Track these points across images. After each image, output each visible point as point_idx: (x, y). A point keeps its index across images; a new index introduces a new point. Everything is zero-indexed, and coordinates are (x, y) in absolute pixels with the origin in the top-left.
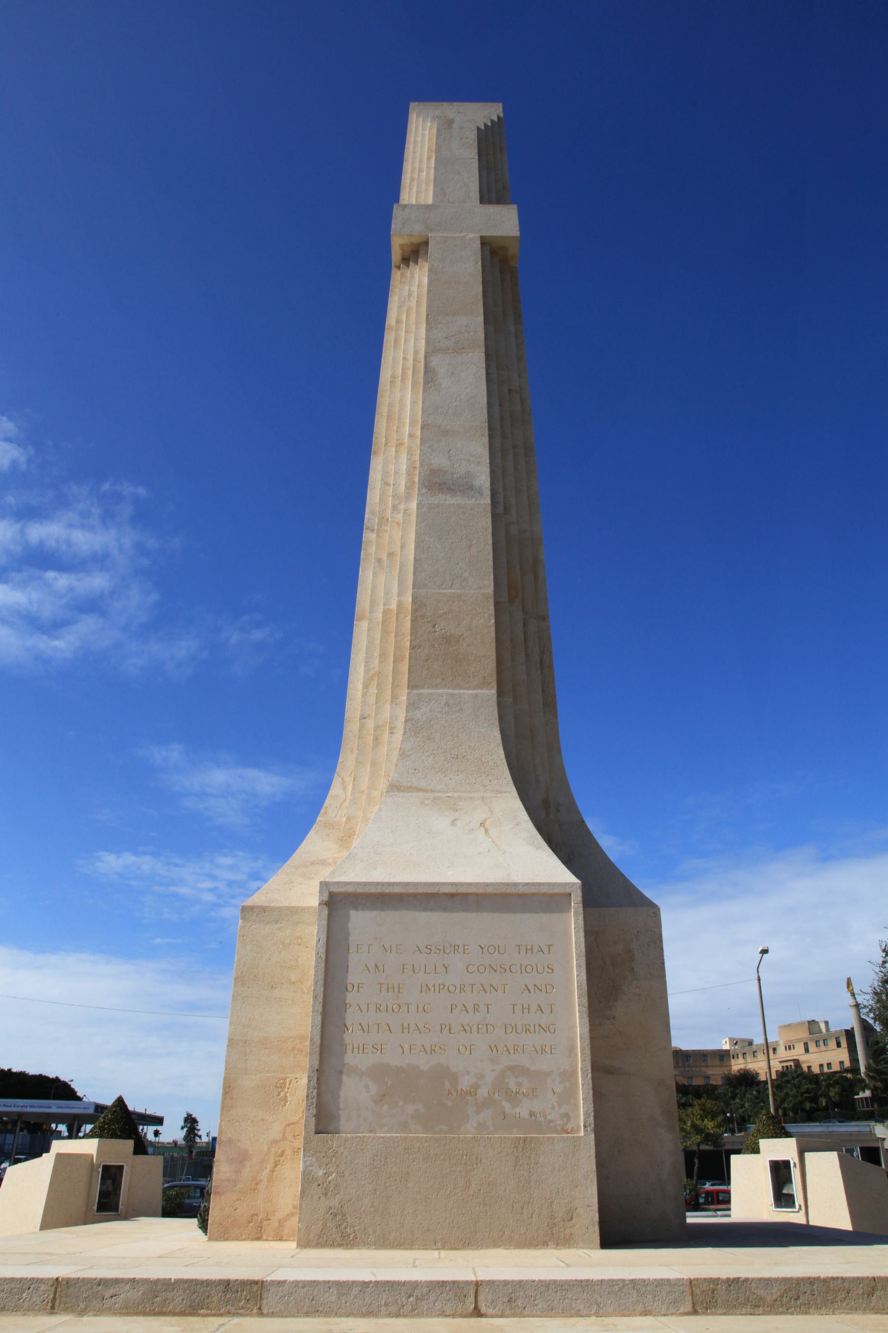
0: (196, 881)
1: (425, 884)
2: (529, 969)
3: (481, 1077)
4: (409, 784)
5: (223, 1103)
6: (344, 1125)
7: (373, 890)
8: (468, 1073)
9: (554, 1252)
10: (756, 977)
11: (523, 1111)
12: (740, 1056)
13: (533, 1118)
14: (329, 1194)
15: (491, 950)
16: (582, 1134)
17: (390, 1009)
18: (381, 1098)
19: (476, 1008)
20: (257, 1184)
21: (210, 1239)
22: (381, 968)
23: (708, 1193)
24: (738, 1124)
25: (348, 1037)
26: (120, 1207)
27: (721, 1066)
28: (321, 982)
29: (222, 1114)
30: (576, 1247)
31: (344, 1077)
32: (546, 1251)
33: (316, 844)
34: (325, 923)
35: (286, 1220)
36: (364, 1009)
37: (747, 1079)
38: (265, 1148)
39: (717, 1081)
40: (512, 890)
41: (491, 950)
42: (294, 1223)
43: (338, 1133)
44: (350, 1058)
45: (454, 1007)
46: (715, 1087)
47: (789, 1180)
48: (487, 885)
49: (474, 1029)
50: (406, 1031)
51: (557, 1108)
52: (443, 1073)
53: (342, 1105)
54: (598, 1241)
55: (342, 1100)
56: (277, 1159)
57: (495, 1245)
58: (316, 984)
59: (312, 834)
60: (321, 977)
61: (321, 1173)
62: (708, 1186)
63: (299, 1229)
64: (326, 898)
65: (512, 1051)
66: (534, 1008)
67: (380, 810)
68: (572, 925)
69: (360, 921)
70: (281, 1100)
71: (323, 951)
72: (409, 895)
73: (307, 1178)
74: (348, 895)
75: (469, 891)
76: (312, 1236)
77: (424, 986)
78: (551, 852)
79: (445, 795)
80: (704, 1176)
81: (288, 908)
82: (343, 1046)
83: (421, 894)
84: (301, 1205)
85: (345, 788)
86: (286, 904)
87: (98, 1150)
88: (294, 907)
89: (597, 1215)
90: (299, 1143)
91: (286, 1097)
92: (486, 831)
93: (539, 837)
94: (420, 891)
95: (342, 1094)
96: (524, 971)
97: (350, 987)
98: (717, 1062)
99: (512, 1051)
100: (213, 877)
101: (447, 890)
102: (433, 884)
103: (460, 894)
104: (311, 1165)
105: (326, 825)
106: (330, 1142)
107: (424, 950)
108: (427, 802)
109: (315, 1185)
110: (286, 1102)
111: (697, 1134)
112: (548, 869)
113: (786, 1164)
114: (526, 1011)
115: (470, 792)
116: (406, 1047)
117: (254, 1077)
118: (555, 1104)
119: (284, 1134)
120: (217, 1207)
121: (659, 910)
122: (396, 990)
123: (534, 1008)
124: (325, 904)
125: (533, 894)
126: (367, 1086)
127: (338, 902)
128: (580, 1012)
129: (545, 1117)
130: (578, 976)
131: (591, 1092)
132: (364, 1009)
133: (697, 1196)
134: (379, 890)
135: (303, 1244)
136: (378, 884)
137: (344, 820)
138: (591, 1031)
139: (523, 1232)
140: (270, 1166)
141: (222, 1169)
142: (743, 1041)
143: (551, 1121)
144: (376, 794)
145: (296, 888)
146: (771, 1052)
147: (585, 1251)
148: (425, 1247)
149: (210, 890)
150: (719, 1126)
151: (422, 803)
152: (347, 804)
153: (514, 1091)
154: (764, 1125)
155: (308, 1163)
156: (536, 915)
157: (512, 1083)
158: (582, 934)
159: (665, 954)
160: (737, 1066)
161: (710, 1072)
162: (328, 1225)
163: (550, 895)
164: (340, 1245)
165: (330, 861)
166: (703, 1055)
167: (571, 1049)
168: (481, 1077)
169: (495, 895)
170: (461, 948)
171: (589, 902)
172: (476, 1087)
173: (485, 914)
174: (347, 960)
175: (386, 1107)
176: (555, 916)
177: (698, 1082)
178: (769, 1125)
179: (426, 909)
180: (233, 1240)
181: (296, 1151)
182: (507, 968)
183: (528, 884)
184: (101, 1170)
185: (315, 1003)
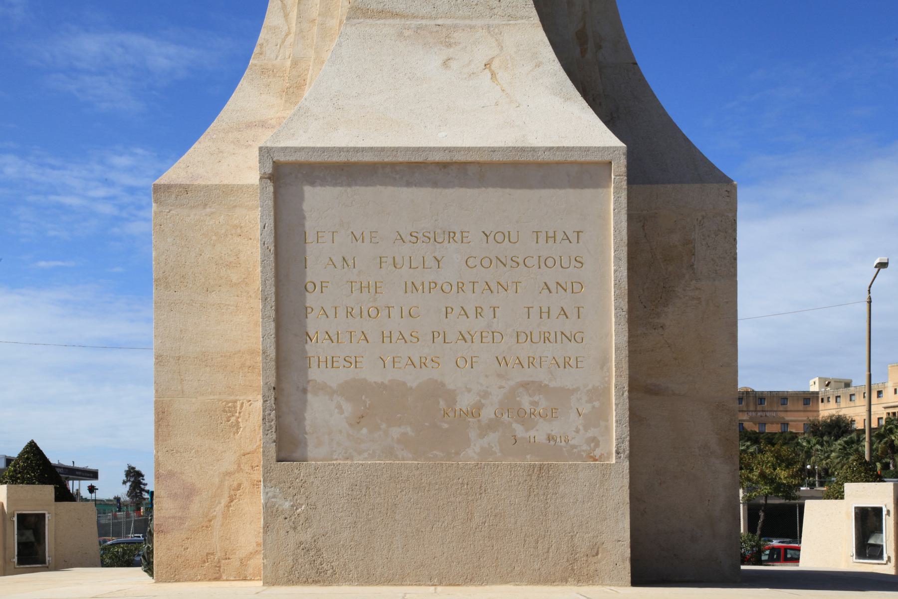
0: (83, 187)
1: (407, 149)
2: (550, 262)
3: (486, 395)
4: (380, 7)
5: (157, 431)
6: (311, 451)
7: (335, 159)
8: (469, 390)
9: (575, 589)
10: (866, 299)
11: (539, 433)
12: (832, 400)
13: (552, 443)
14: (299, 528)
15: (499, 237)
16: (614, 461)
17: (365, 313)
18: (359, 420)
19: (479, 312)
20: (210, 521)
21: (158, 581)
22: (351, 263)
23: (773, 550)
24: (820, 477)
25: (310, 348)
26: (47, 559)
27: (805, 411)
28: (271, 281)
29: (157, 444)
30: (602, 584)
31: (310, 396)
32: (565, 587)
33: (249, 100)
34: (271, 203)
35: (249, 559)
36: (331, 313)
37: (839, 427)
38: (216, 480)
39: (796, 428)
40: (530, 158)
41: (499, 237)
42: (258, 561)
43: (305, 460)
44: (315, 374)
45: (449, 310)
46: (794, 436)
47: (879, 529)
48: (493, 150)
49: (477, 338)
50: (387, 340)
51: (582, 431)
52: (435, 392)
53: (308, 428)
54: (628, 578)
55: (308, 423)
56: (232, 493)
57: (503, 579)
58: (264, 283)
59: (244, 84)
60: (271, 274)
61: (287, 505)
62: (775, 543)
63: (265, 566)
64: (269, 170)
65: (526, 365)
66: (555, 312)
67: (340, 45)
68: (611, 204)
69: (317, 201)
70: (231, 426)
71: (270, 240)
72: (384, 165)
73: (270, 512)
74: (299, 166)
75: (469, 159)
76: (281, 572)
77: (409, 285)
78: (585, 104)
79: (433, 22)
80: (769, 533)
81: (217, 187)
82: (305, 357)
83: (401, 163)
84: (264, 540)
85: (286, 16)
86: (216, 181)
87: (8, 498)
88: (228, 186)
89: (629, 551)
90: (258, 475)
91: (238, 422)
92: (493, 75)
93: (569, 83)
94: (400, 159)
95: (308, 416)
96: (542, 265)
97: (310, 287)
98: (801, 406)
99: (526, 365)
100: (107, 183)
101: (437, 157)
102: (418, 149)
103: (455, 163)
104: (274, 497)
105: (264, 71)
106: (296, 471)
107: (408, 238)
108: (407, 33)
109: (281, 518)
110: (238, 428)
111: (766, 484)
112: (581, 128)
113: (878, 511)
114: (545, 315)
115: (469, 18)
116: (389, 360)
117: (194, 400)
118: (581, 427)
119: (239, 466)
120: (161, 549)
121: (735, 188)
122: (372, 290)
123: (555, 312)
124: (269, 178)
125: (558, 163)
126: (339, 407)
127: (287, 176)
128: (616, 317)
129: (567, 441)
130: (615, 271)
131: (628, 413)
132: (331, 313)
133: (760, 552)
134: (342, 158)
135: (272, 581)
136: (341, 149)
137: (288, 63)
138: (630, 342)
139: (537, 567)
140: (224, 501)
141: (164, 510)
142: (838, 381)
143: (574, 447)
144: (333, 23)
145: (228, 158)
146: (874, 395)
147: (612, 588)
148: (418, 583)
149: (107, 199)
150: (793, 476)
151: (400, 34)
152: (290, 39)
153: (528, 411)
154: (853, 472)
155: (270, 494)
156: (561, 192)
157: (525, 402)
158: (624, 217)
159: (738, 246)
160: (826, 411)
161: (789, 417)
162: (300, 561)
163: (582, 164)
164: (315, 582)
165: (273, 122)
166: (783, 398)
167: (604, 362)
168: (486, 395)
169: (505, 164)
170: (458, 235)
171: (636, 175)
172: (479, 407)
173: (491, 190)
174: (304, 251)
175: (365, 431)
176: (588, 193)
177: (772, 428)
178: (860, 472)
179: (408, 184)
180: (186, 581)
181: (255, 484)
182: (520, 260)
183: (550, 149)
184: (15, 519)
185: (264, 307)
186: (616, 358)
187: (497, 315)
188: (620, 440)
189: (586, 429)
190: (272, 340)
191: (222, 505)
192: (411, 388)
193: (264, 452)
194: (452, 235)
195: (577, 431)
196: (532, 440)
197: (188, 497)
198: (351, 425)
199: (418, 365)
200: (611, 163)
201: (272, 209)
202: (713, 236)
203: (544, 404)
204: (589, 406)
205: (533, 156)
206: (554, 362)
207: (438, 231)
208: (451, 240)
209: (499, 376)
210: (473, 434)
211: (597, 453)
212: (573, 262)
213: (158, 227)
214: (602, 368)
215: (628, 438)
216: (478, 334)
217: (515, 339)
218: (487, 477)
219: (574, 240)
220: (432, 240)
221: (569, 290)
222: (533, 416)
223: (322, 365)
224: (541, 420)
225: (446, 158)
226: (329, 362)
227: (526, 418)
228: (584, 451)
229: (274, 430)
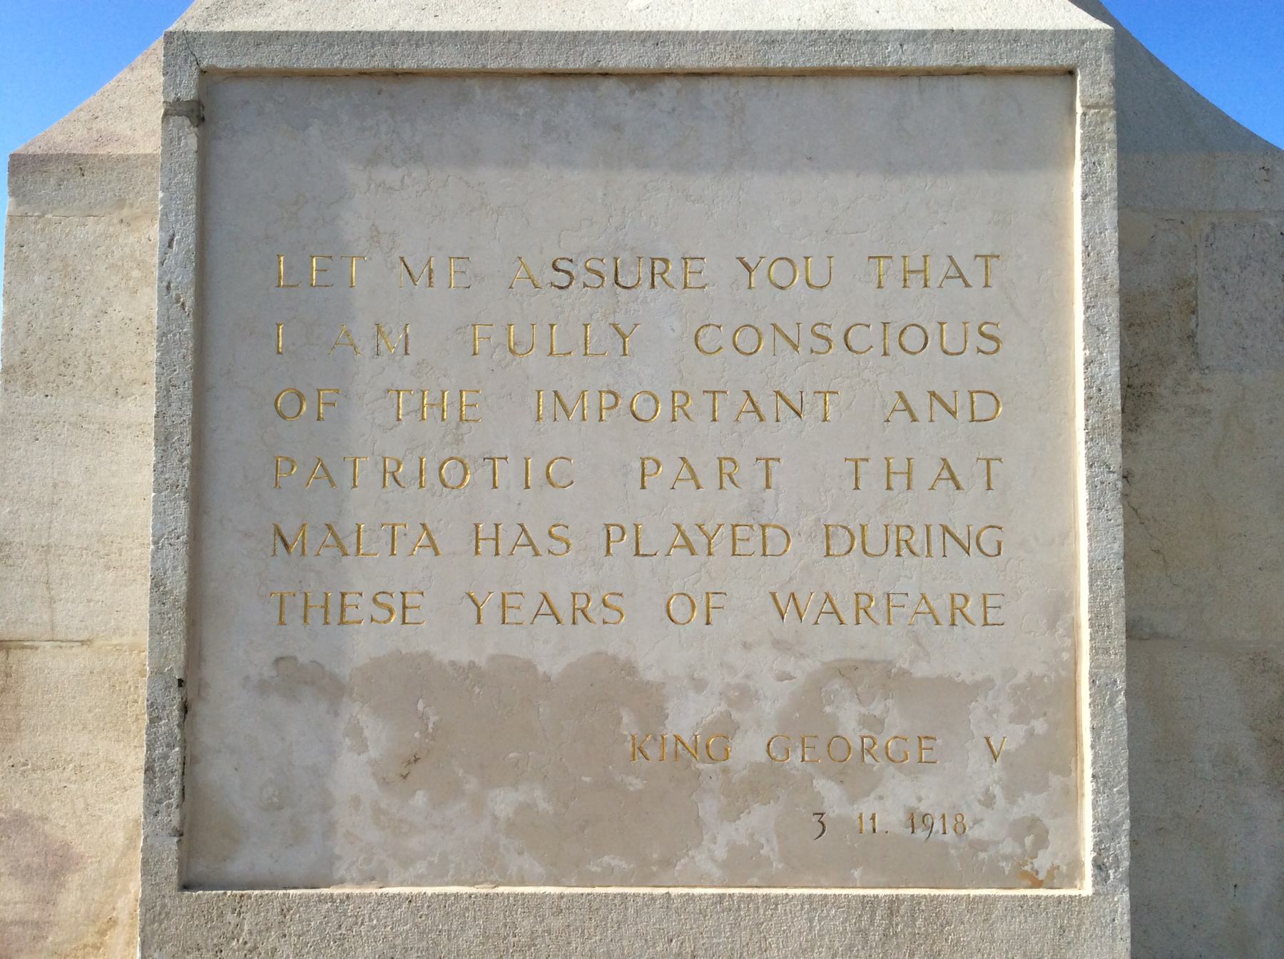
1: (547, 37)
2: (913, 339)
8: (700, 685)
13: (921, 834)
17: (430, 477)
19: (726, 473)
34: (189, 179)
45: (650, 465)
49: (722, 543)
50: (486, 547)
51: (1000, 801)
52: (615, 689)
65: (849, 617)
71: (184, 279)
102: (574, 38)
106: (231, 918)
114: (899, 481)
118: (996, 790)
123: (927, 471)
128: (1092, 486)
129: (961, 830)
130: (1088, 363)
136: (375, 38)
153: (856, 744)
157: (848, 718)
167: (1060, 607)
172: (725, 731)
175: (420, 798)
182: (836, 335)
185: (162, 458)
186: (1093, 600)
187: (773, 481)
188: (1105, 829)
189: (1012, 795)
190: (177, 556)
191: (132, 896)
192: (547, 679)
193: (145, 862)
194: (659, 266)
195: (988, 801)
196: (867, 827)
197: (55, 875)
198: (384, 783)
199: (566, 615)
200: (1071, 73)
201: (192, 196)
202: (1236, 269)
203: (897, 722)
204: (1020, 730)
205: (872, 54)
206: (923, 608)
207: (624, 256)
208: (658, 280)
209: (780, 645)
210: (708, 807)
211: (1043, 862)
212: (975, 339)
213: (16, 250)
214: (1052, 626)
215: (1126, 826)
216: (725, 531)
217: (819, 547)
218: (745, 935)
219: (976, 278)
220: (609, 279)
221: (963, 415)
222: (868, 759)
223: (316, 614)
224: (892, 769)
225: (647, 60)
226: (334, 610)
227: (847, 763)
228: (1006, 858)
229: (174, 801)
